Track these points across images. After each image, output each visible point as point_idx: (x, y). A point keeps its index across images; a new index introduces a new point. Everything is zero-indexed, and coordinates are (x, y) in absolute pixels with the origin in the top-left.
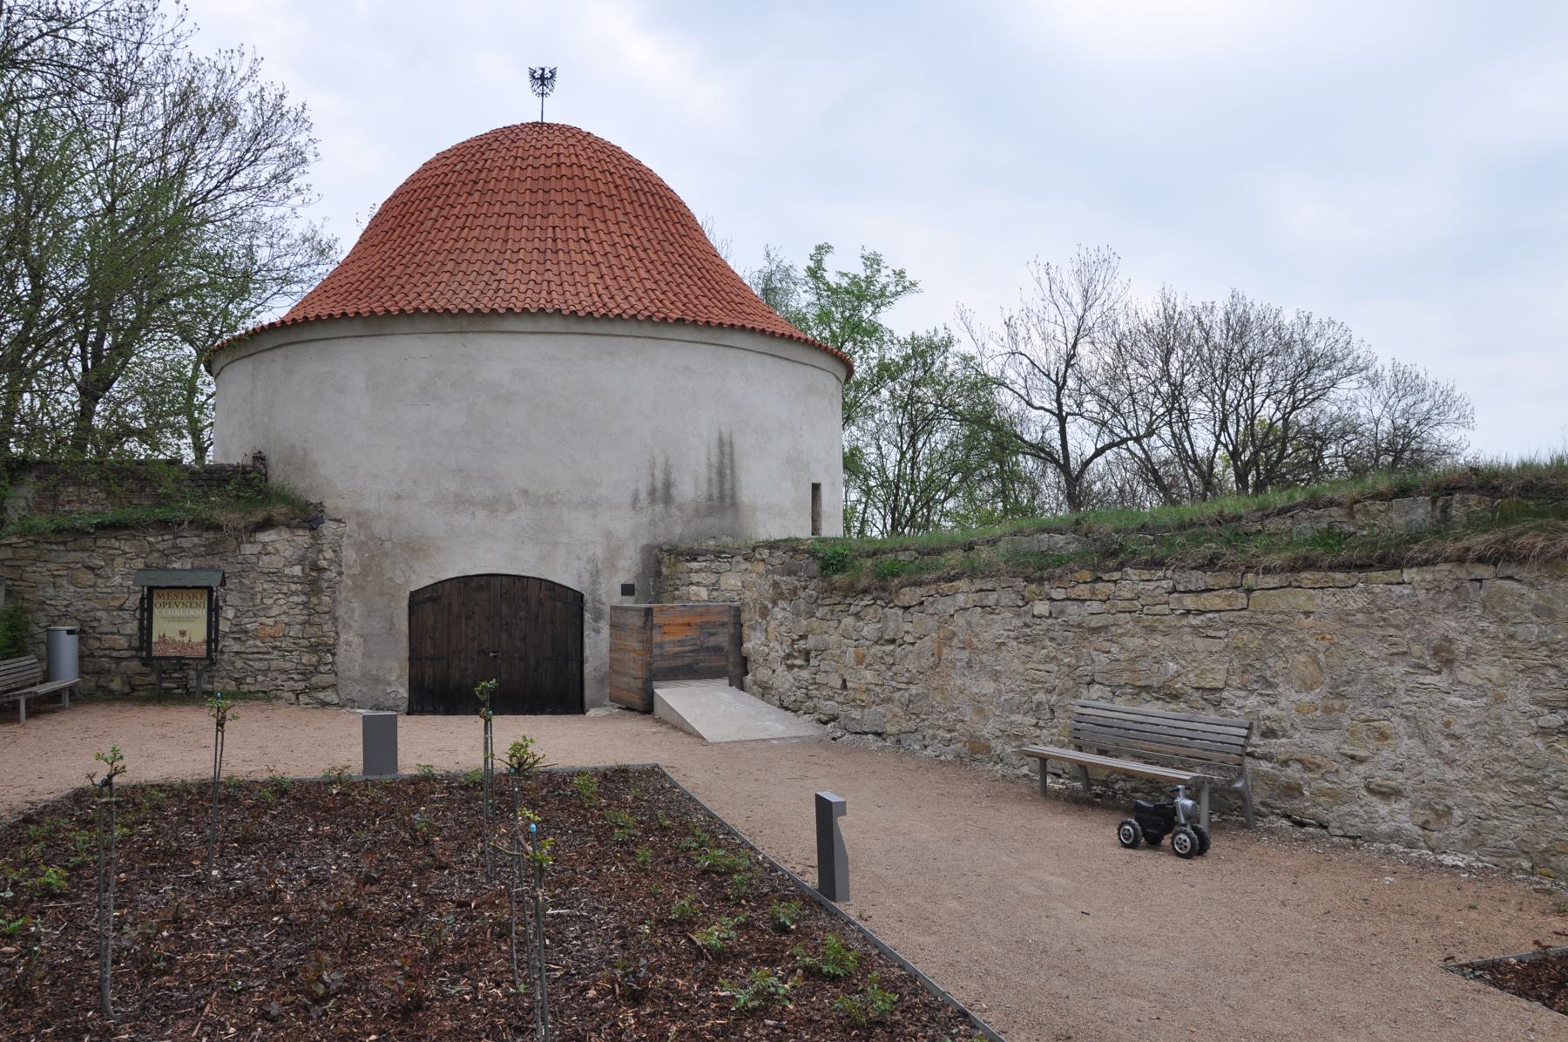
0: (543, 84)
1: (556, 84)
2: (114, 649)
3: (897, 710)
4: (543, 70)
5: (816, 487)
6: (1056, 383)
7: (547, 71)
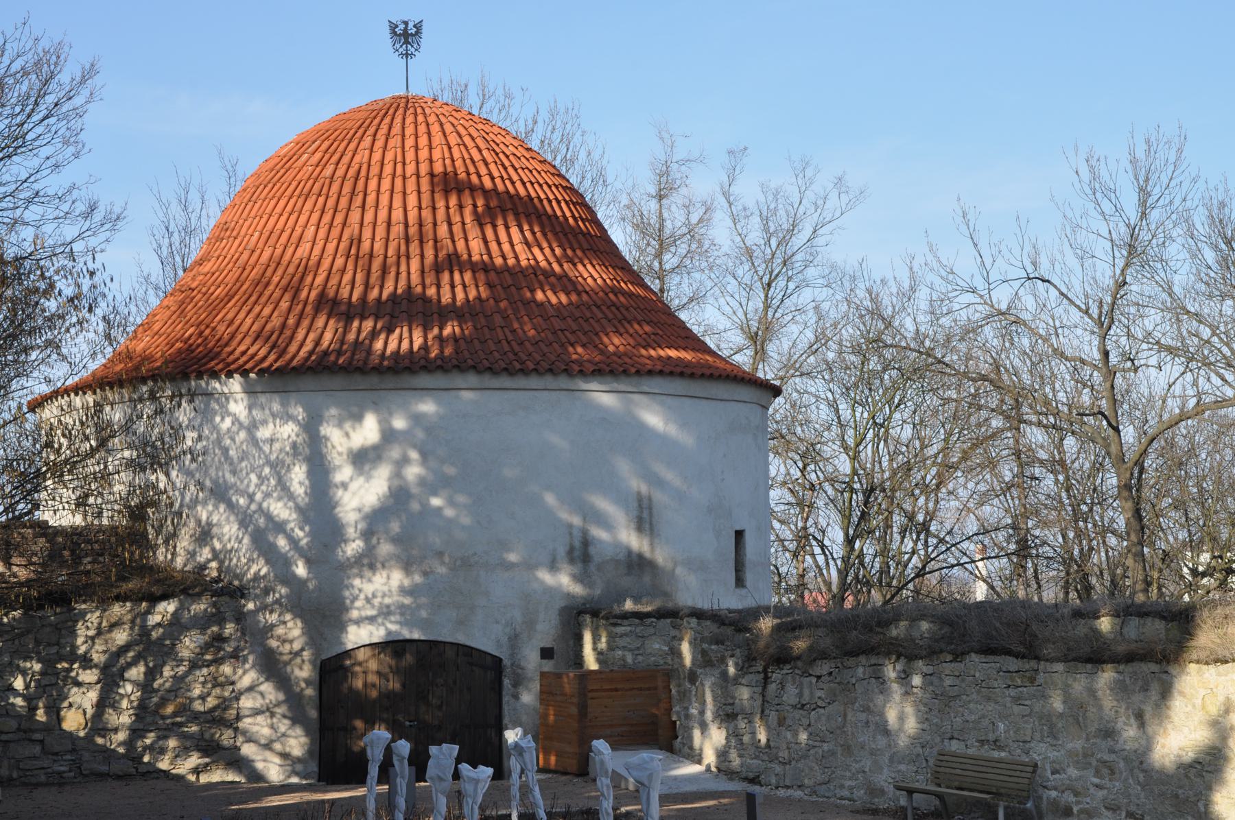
0: (407, 42)
1: (423, 42)
3: (814, 764)
4: (406, 23)
5: (739, 534)
7: (411, 25)
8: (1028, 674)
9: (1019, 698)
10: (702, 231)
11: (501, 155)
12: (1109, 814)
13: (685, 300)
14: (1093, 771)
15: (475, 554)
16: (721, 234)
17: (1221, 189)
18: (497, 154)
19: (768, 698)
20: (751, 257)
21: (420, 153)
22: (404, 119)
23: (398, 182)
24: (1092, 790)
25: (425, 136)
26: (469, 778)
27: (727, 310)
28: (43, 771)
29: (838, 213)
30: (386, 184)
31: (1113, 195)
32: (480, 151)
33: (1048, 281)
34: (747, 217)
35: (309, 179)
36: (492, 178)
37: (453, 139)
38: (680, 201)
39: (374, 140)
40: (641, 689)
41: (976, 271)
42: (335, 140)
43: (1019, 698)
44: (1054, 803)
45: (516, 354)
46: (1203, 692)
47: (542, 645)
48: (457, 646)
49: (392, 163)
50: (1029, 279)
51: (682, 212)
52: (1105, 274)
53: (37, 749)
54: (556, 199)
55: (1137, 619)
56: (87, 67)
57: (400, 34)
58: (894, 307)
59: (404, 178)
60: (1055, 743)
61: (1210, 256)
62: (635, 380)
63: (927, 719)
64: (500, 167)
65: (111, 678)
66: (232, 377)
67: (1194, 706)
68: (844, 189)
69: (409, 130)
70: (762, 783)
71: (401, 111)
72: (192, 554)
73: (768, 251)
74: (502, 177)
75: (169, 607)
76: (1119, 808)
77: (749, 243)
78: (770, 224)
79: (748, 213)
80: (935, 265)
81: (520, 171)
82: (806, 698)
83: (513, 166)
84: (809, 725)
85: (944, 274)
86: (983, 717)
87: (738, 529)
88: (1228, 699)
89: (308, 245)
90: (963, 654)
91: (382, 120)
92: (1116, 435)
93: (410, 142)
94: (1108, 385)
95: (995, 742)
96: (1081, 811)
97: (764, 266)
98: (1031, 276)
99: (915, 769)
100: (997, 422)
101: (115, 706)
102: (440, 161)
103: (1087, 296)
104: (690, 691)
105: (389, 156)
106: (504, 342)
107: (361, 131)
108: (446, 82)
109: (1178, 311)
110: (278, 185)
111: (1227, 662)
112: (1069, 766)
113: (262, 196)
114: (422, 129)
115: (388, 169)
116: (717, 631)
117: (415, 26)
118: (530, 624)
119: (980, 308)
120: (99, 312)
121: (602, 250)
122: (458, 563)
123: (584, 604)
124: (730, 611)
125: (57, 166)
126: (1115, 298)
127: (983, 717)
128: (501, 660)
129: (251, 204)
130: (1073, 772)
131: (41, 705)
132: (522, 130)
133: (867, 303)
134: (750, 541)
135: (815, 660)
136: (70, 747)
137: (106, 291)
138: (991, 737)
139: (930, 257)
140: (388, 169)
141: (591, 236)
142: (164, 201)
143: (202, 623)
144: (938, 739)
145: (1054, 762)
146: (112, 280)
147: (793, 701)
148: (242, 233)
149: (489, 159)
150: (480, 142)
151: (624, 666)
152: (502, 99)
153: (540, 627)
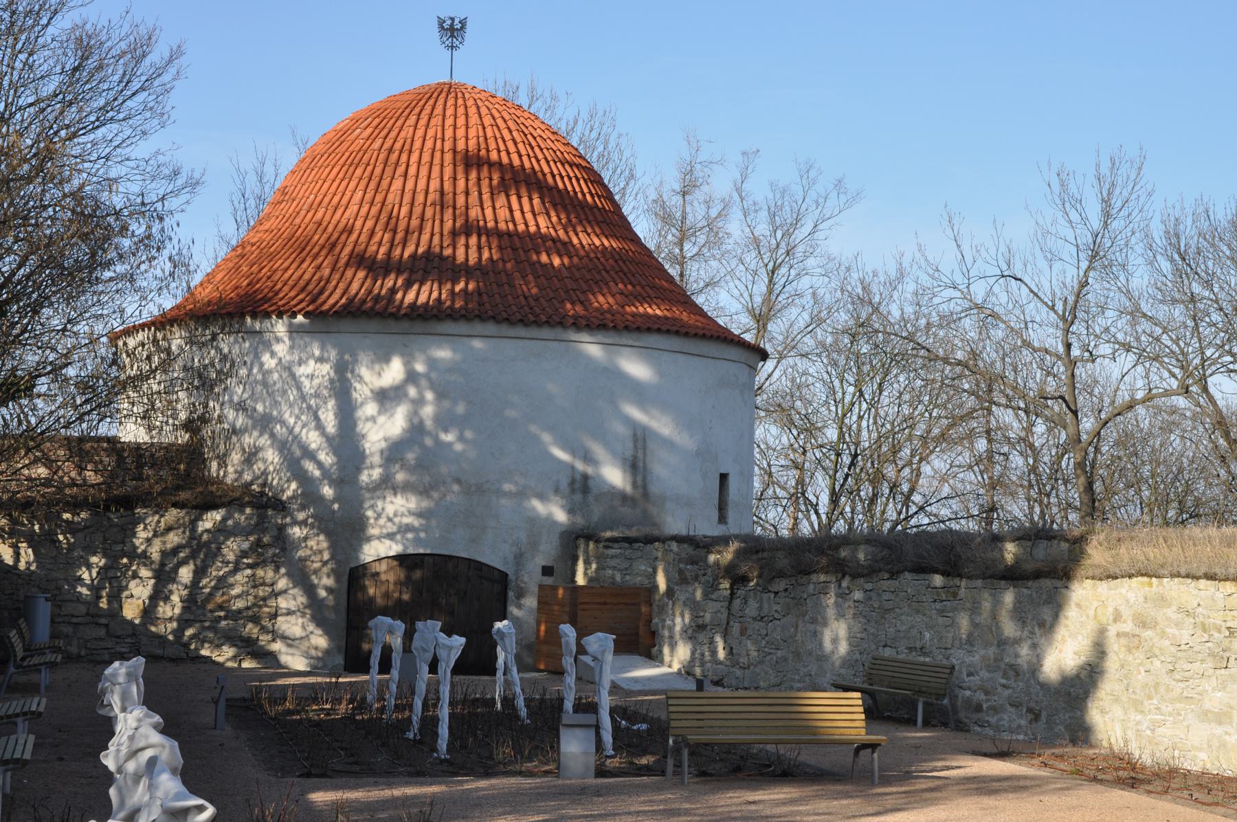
0: (452, 36)
1: (467, 35)
2: (73, 616)
4: (453, 19)
5: (724, 477)
6: (1063, 318)
7: (457, 21)
8: (951, 590)
9: (943, 611)
10: (720, 224)
11: (529, 136)
12: (1012, 710)
13: (702, 284)
14: (1001, 673)
15: (488, 481)
16: (735, 228)
17: (1178, 207)
18: (526, 135)
19: (733, 612)
20: (758, 246)
21: (457, 131)
22: (446, 102)
23: (438, 155)
24: (1000, 689)
25: (463, 117)
26: (443, 645)
27: (736, 292)
28: (106, 651)
29: (837, 212)
30: (426, 157)
31: (1078, 205)
32: (511, 132)
33: (1020, 280)
34: (756, 211)
35: (359, 151)
36: (520, 156)
37: (487, 121)
38: (702, 199)
39: (418, 119)
40: (626, 604)
41: (956, 267)
42: (384, 118)
43: (943, 611)
44: (968, 701)
45: (531, 309)
46: (1095, 604)
47: (544, 563)
48: (470, 561)
49: (432, 139)
50: (1003, 276)
51: (702, 206)
52: (1072, 276)
53: (102, 632)
54: (576, 177)
55: (1045, 542)
56: (175, 49)
57: (447, 29)
58: (881, 294)
59: (443, 152)
60: (971, 649)
61: (1166, 266)
62: (635, 335)
63: (865, 629)
64: (528, 147)
65: (164, 577)
66: (282, 318)
67: (1088, 616)
68: (842, 190)
69: (450, 112)
70: (725, 684)
71: (444, 95)
72: (240, 473)
73: (773, 242)
74: (529, 155)
75: (216, 516)
76: (1021, 705)
77: (756, 234)
78: (777, 218)
79: (757, 208)
80: (923, 264)
81: (545, 151)
82: (765, 611)
83: (539, 146)
84: (767, 635)
85: (931, 272)
86: (913, 627)
87: (723, 472)
88: (1116, 609)
89: (356, 208)
90: (898, 572)
91: (427, 102)
92: (1074, 421)
93: (449, 122)
94: (1069, 373)
95: (921, 649)
96: (990, 708)
97: (769, 254)
98: (1006, 273)
99: (853, 672)
100: (971, 402)
101: (167, 599)
102: (475, 139)
103: (1054, 295)
104: (667, 605)
105: (431, 133)
106: (522, 299)
107: (408, 111)
108: (500, 83)
109: (1135, 313)
110: (333, 155)
111: (1117, 578)
112: (981, 669)
113: (319, 164)
114: (461, 110)
115: (429, 144)
116: (693, 553)
117: (460, 22)
118: (534, 545)
119: (959, 301)
120: (166, 253)
121: (614, 223)
122: (473, 489)
123: (582, 530)
124: (705, 537)
125: (144, 133)
126: (1078, 296)
127: (913, 627)
128: (507, 575)
129: (309, 171)
130: (984, 674)
131: (104, 594)
132: (564, 128)
133: (859, 290)
134: (733, 483)
135: (773, 578)
136: (130, 632)
137: (173, 235)
138: (918, 645)
139: (918, 255)
140: (429, 144)
141: (605, 210)
142: (242, 171)
143: (245, 532)
144: (874, 647)
145: (970, 665)
146: (178, 225)
147: (754, 613)
148: (300, 196)
149: (518, 139)
150: (511, 124)
151: (613, 584)
152: (549, 100)
153: (542, 548)
